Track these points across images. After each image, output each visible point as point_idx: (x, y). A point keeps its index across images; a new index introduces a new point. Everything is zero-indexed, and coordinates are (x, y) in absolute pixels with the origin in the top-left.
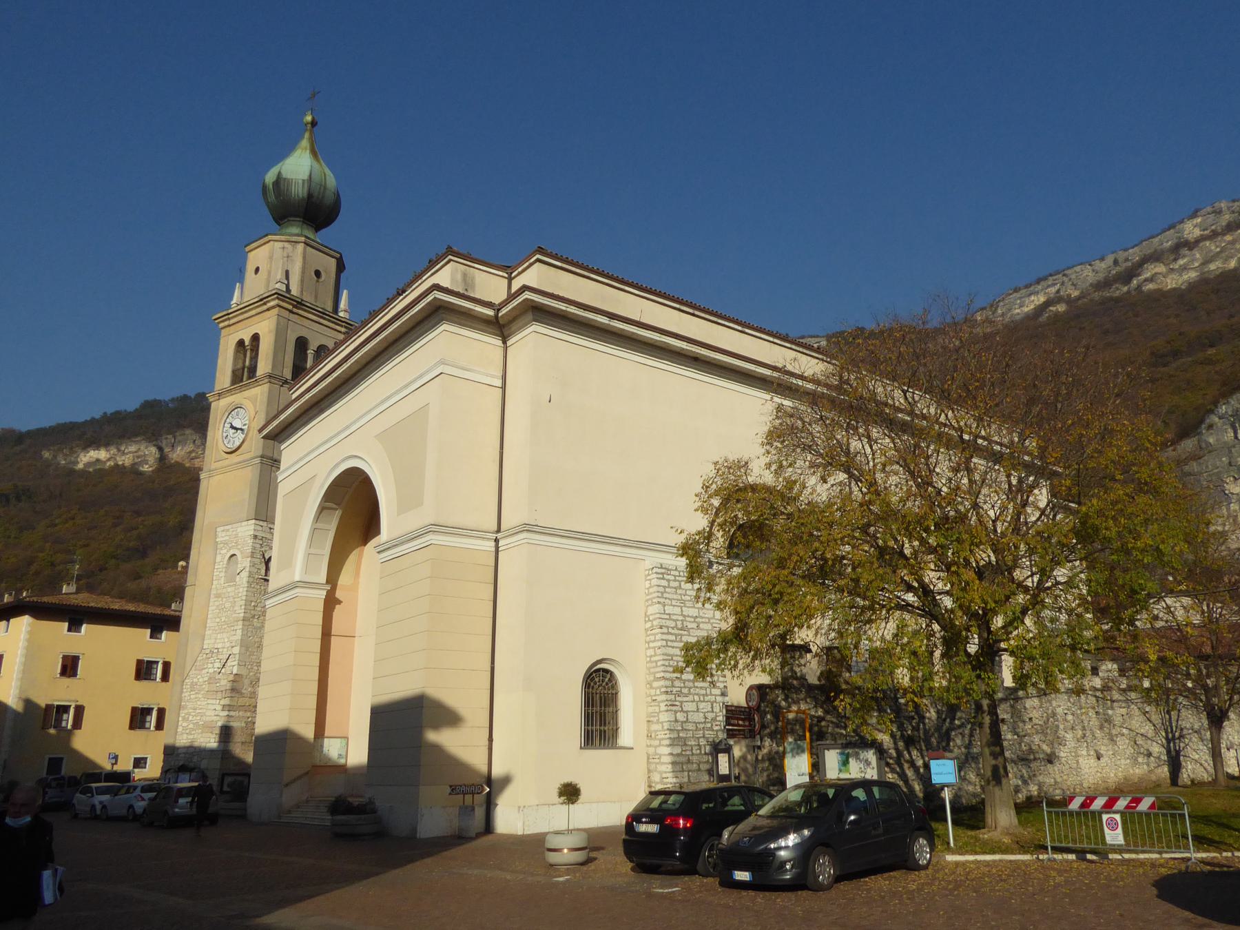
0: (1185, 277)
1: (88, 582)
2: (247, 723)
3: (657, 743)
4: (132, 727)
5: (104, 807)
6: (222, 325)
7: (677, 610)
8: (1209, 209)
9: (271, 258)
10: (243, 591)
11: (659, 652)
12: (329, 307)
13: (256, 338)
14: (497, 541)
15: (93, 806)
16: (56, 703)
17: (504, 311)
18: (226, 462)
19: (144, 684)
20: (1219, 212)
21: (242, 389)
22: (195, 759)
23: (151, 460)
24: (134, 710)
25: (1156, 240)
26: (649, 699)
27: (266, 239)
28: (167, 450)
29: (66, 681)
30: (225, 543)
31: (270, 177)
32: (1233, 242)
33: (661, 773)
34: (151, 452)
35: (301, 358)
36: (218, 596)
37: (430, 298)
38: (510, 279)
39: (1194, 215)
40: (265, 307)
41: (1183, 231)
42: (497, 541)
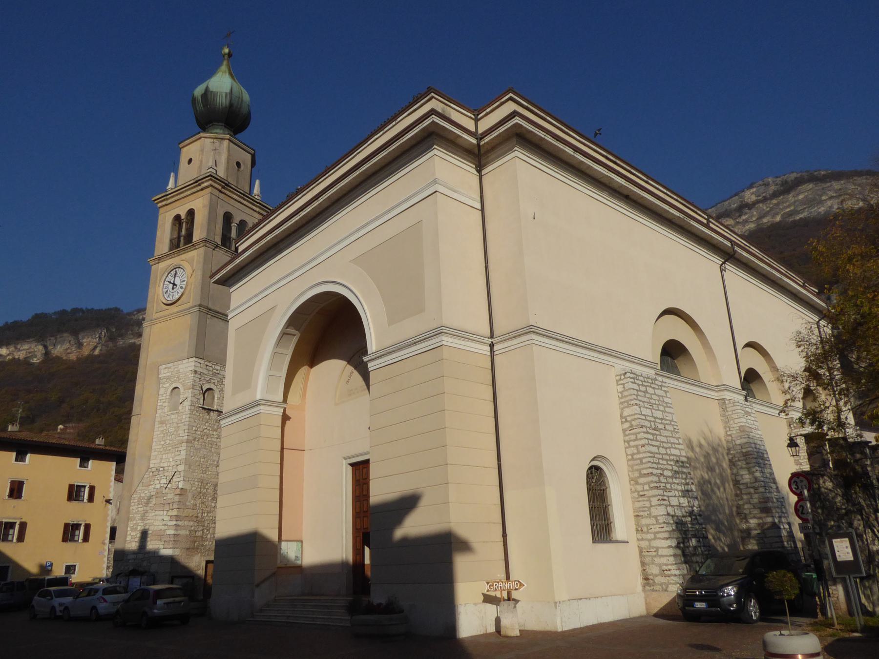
0: (747, 227)
1: (27, 421)
2: (190, 531)
3: (651, 536)
4: (65, 540)
5: (66, 608)
6: (159, 205)
7: (648, 412)
8: (761, 182)
9: (202, 150)
10: (185, 418)
11: (642, 449)
12: (247, 189)
13: (191, 213)
14: (492, 346)
15: (53, 608)
16: (4, 521)
17: (487, 139)
18: (166, 313)
19: (74, 504)
20: (767, 185)
21: (179, 253)
22: (145, 564)
23: (39, 355)
24: (67, 526)
25: (727, 203)
26: (636, 495)
27: (197, 136)
28: (50, 348)
29: (14, 502)
30: (168, 378)
31: (199, 91)
32: (778, 204)
33: (660, 565)
34: (39, 349)
35: (229, 232)
36: (162, 423)
37: (427, 122)
38: (477, 120)
39: (751, 187)
40: (199, 188)
41: (743, 197)
42: (492, 346)
